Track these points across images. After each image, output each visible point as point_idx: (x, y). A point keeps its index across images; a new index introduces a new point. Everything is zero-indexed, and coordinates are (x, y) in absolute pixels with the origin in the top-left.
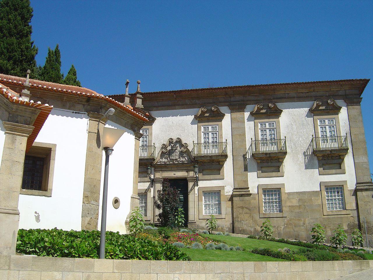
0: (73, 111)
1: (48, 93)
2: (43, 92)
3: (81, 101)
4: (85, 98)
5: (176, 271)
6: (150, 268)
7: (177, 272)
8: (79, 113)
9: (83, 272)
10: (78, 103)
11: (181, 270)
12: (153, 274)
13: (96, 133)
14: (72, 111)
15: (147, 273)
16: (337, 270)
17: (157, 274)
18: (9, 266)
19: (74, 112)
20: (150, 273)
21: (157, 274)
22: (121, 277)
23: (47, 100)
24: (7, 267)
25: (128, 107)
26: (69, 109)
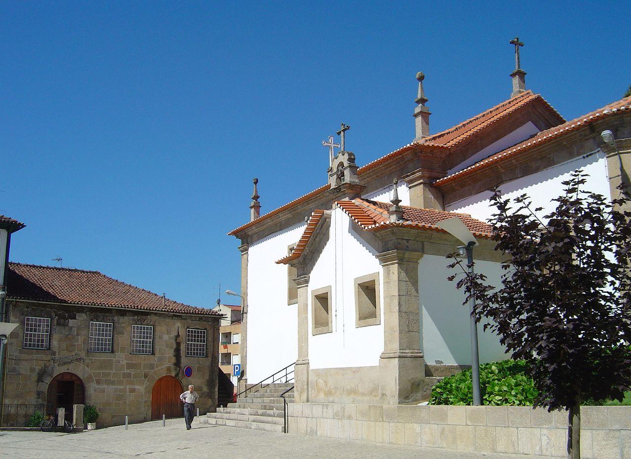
0: (583, 155)
1: (543, 147)
2: (538, 150)
3: (586, 136)
4: (586, 129)
5: (543, 424)
6: (508, 419)
7: (544, 426)
8: (590, 155)
9: (225, 425)
10: (586, 140)
11: (550, 423)
12: (512, 429)
13: (619, 176)
14: (581, 156)
15: (505, 427)
16: (372, 420)
17: (517, 428)
18: (382, 418)
19: (585, 155)
20: (508, 427)
21: (517, 428)
22: (476, 432)
23: (550, 157)
24: (381, 419)
25: (623, 106)
26: (578, 155)
